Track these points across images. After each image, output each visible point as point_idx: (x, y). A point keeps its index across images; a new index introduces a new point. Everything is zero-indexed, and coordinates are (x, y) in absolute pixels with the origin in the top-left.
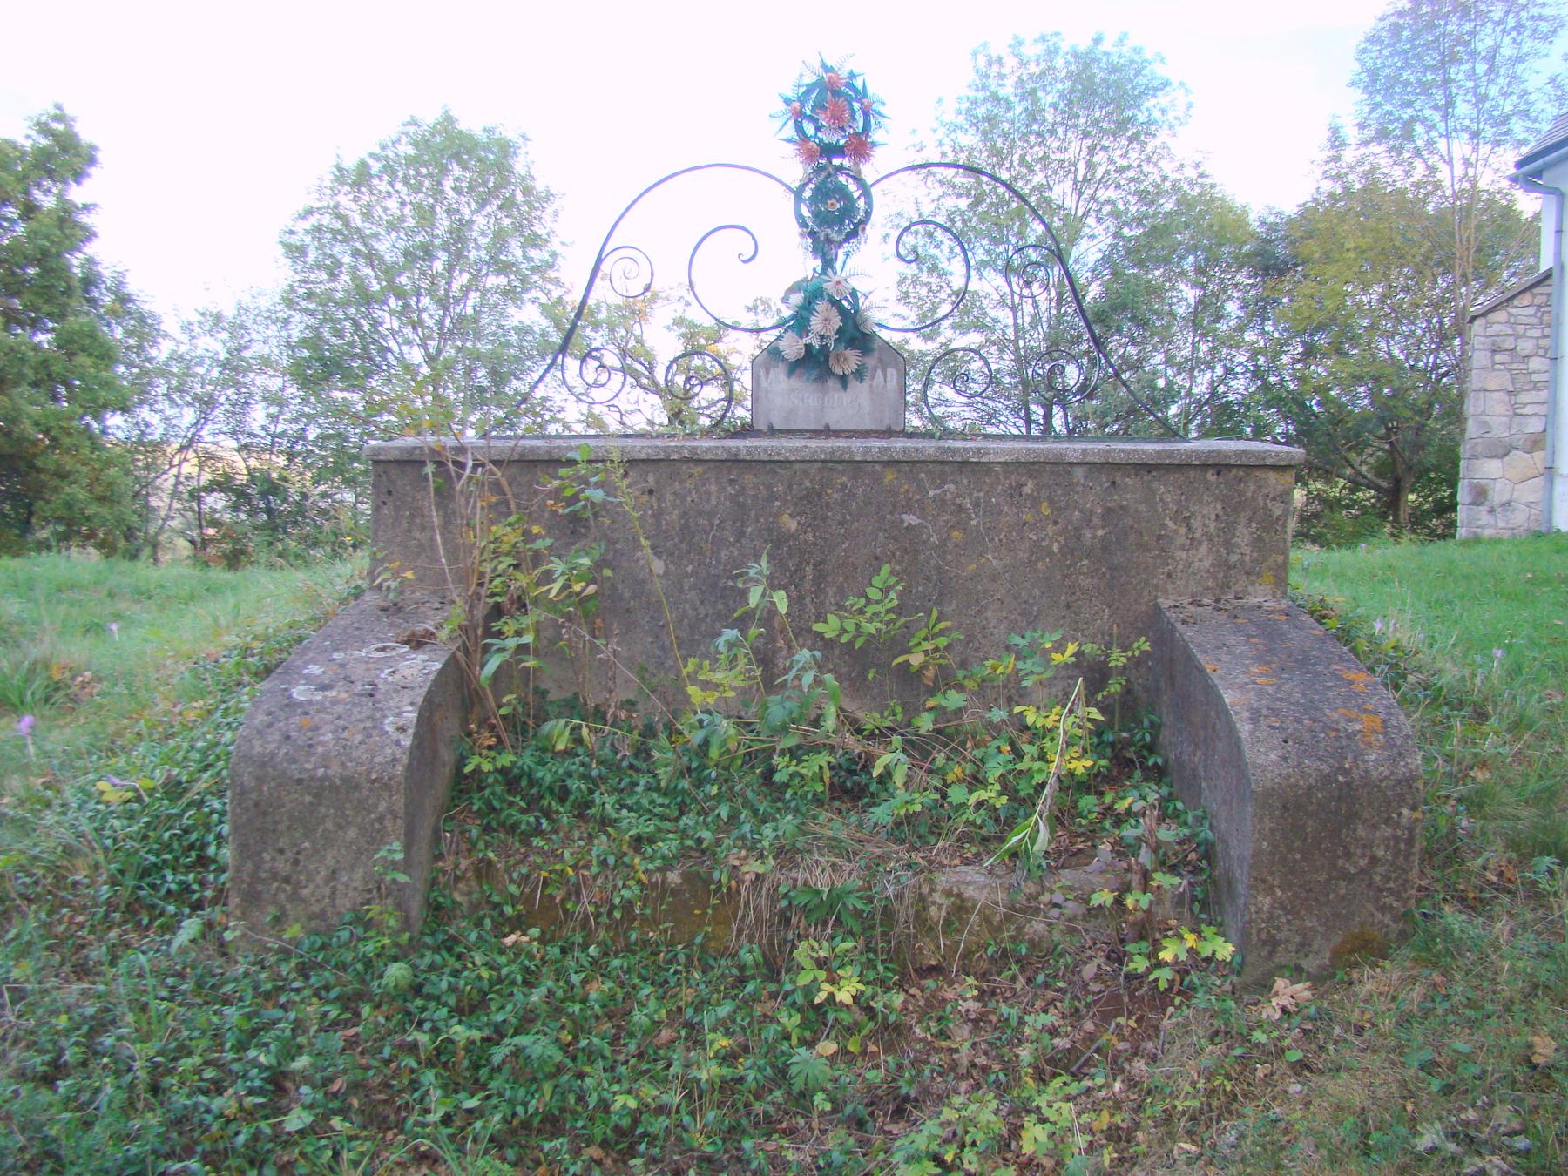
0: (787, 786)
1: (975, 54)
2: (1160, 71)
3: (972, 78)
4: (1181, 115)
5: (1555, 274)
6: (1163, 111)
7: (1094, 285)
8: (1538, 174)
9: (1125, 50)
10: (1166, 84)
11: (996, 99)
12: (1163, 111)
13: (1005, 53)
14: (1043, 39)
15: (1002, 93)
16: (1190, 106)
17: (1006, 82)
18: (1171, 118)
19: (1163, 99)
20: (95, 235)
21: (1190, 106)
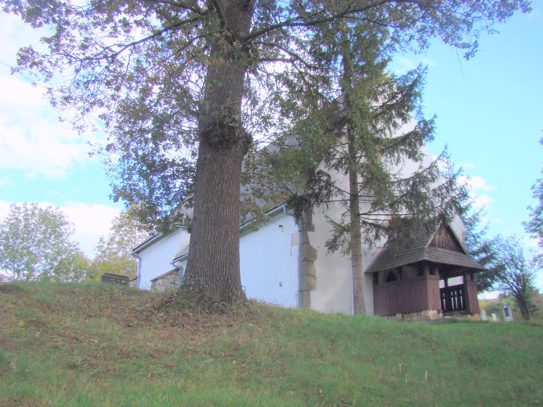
0: (194, 140)
1: (11, 206)
2: (66, 220)
3: (9, 212)
4: (72, 231)
5: (138, 278)
6: (66, 230)
7: (284, 65)
8: (138, 253)
9: (58, 211)
10: (67, 223)
11: (17, 219)
12: (66, 230)
13: (21, 206)
14: (33, 204)
15: (19, 218)
16: (74, 229)
17: (21, 215)
18: (69, 231)
19: (66, 227)
20: (314, 231)
21: (74, 229)
